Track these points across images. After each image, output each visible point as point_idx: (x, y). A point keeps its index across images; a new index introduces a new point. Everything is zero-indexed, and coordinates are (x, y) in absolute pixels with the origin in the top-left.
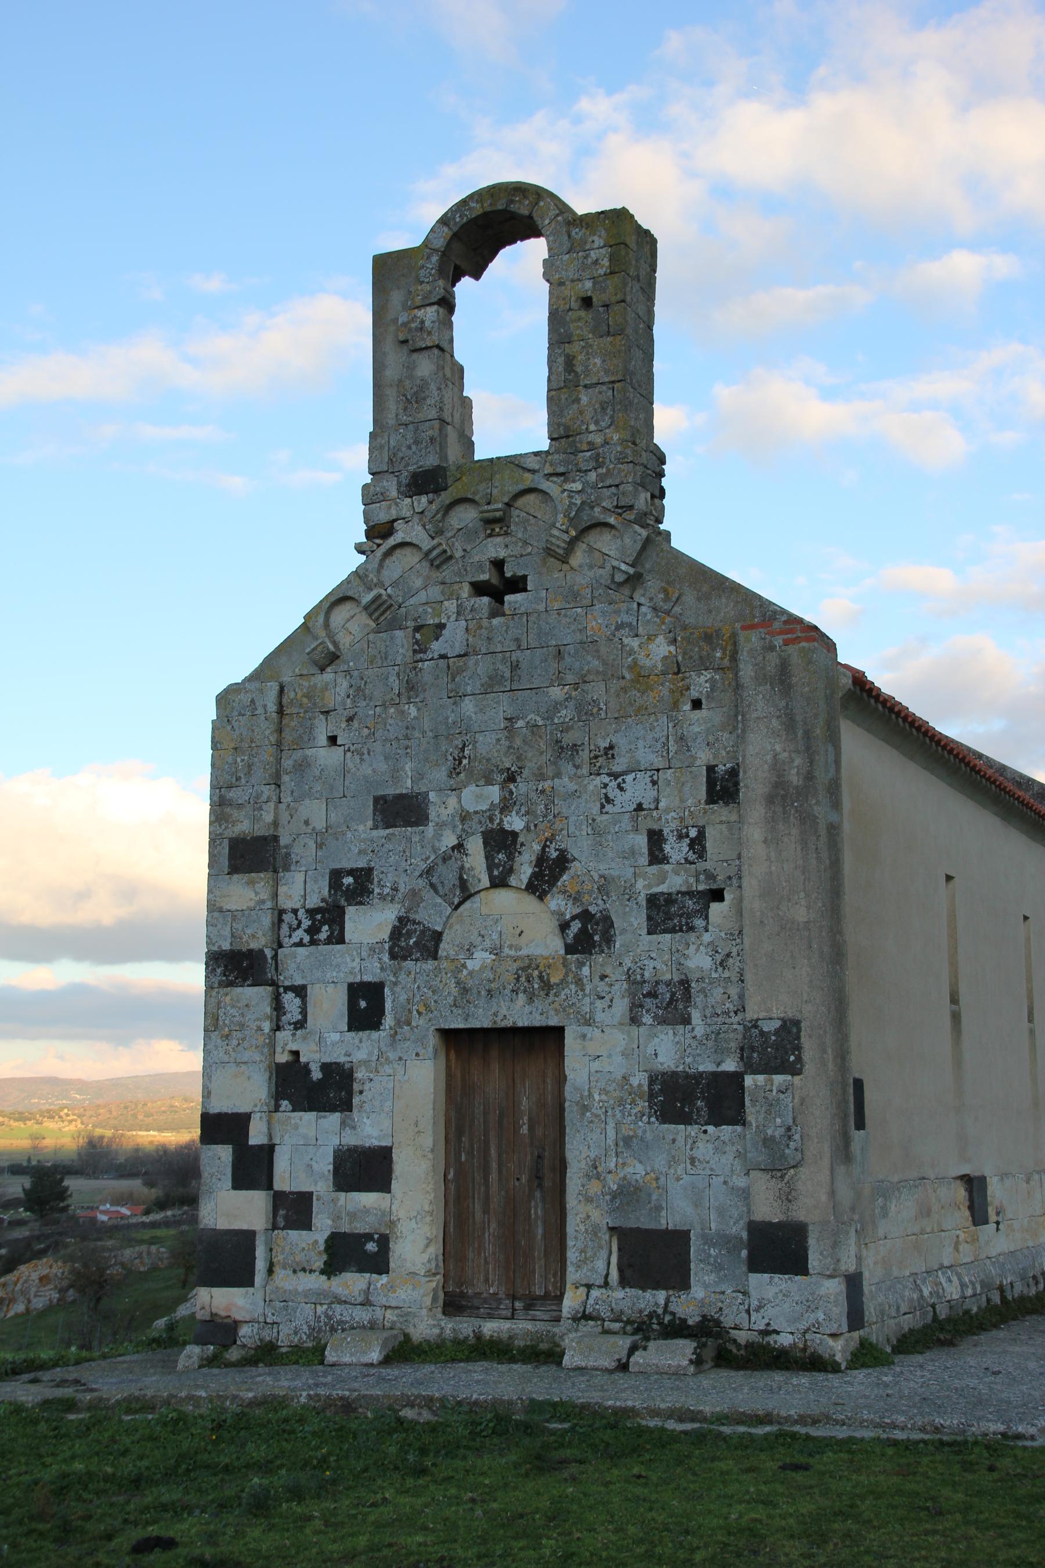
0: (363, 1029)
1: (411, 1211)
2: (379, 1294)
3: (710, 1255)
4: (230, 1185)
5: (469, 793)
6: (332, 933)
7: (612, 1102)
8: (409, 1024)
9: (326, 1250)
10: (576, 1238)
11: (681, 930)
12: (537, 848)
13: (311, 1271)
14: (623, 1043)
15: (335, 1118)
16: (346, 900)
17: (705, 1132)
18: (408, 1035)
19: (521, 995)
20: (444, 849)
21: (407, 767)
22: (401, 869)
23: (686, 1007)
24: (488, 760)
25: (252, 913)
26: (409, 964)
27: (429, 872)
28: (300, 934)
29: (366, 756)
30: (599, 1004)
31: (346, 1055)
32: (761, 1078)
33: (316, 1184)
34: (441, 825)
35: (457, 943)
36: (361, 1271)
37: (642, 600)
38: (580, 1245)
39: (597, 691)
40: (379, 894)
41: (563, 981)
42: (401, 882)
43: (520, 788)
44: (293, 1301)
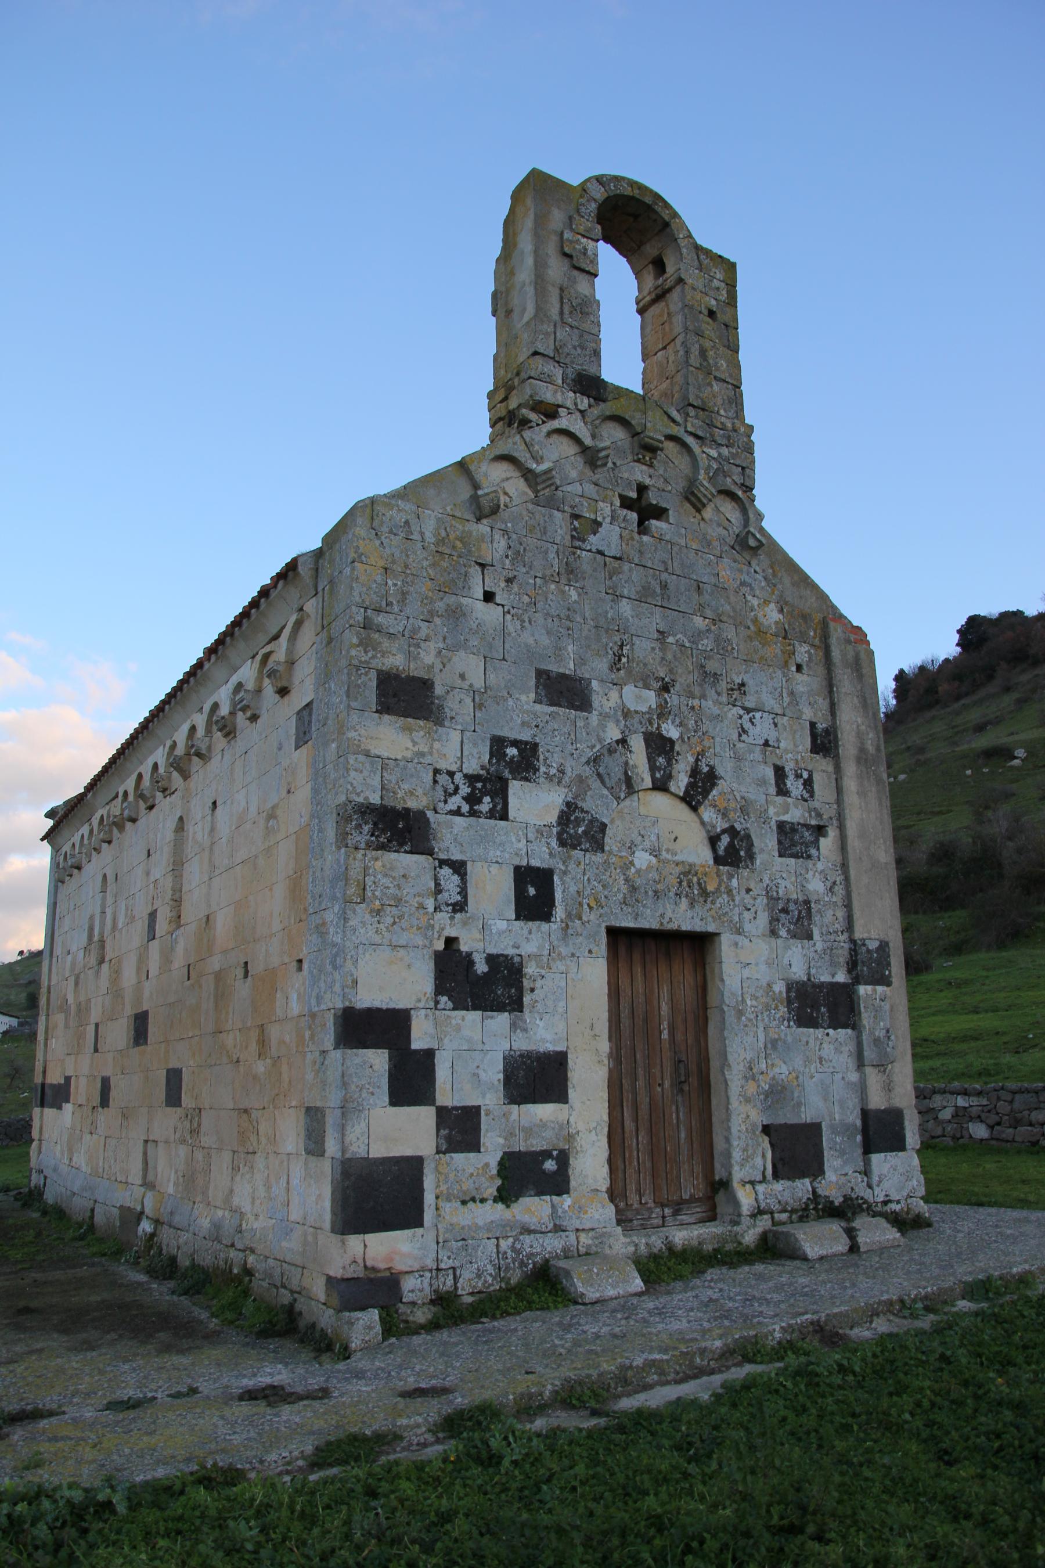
0: (532, 920)
1: (583, 1120)
2: (571, 1217)
3: (836, 1143)
4: (387, 1099)
5: (629, 690)
6: (495, 806)
7: (760, 1007)
8: (580, 918)
9: (499, 1174)
10: (739, 1138)
11: (802, 857)
12: (691, 760)
13: (483, 1201)
14: (767, 953)
15: (501, 1020)
16: (510, 772)
17: (828, 1034)
18: (579, 930)
19: (683, 899)
20: (609, 741)
21: (570, 648)
22: (567, 752)
23: (809, 924)
24: (645, 665)
25: (410, 765)
26: (577, 854)
27: (596, 760)
28: (455, 801)
29: (527, 624)
30: (746, 914)
31: (514, 947)
32: (869, 988)
33: (484, 1096)
34: (604, 716)
35: (618, 839)
36: (540, 1193)
37: (757, 569)
38: (743, 1144)
39: (730, 632)
40: (545, 773)
41: (718, 890)
42: (568, 765)
43: (673, 699)
44: (473, 1238)
